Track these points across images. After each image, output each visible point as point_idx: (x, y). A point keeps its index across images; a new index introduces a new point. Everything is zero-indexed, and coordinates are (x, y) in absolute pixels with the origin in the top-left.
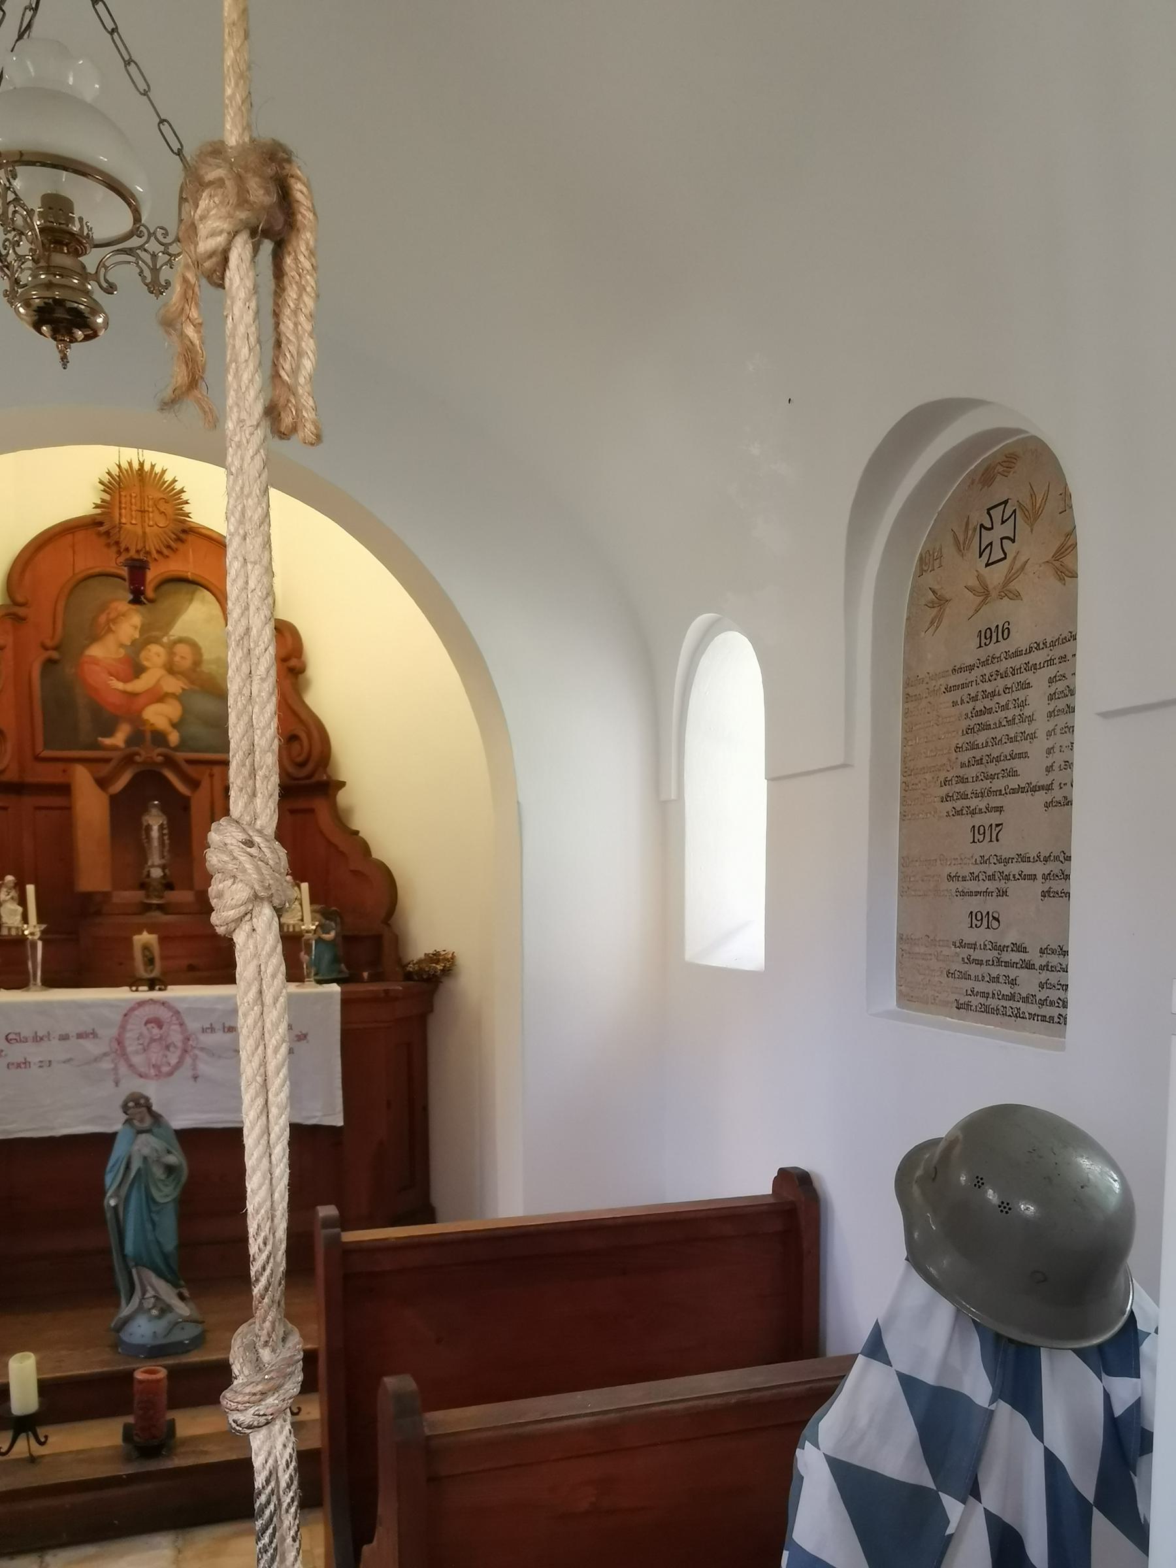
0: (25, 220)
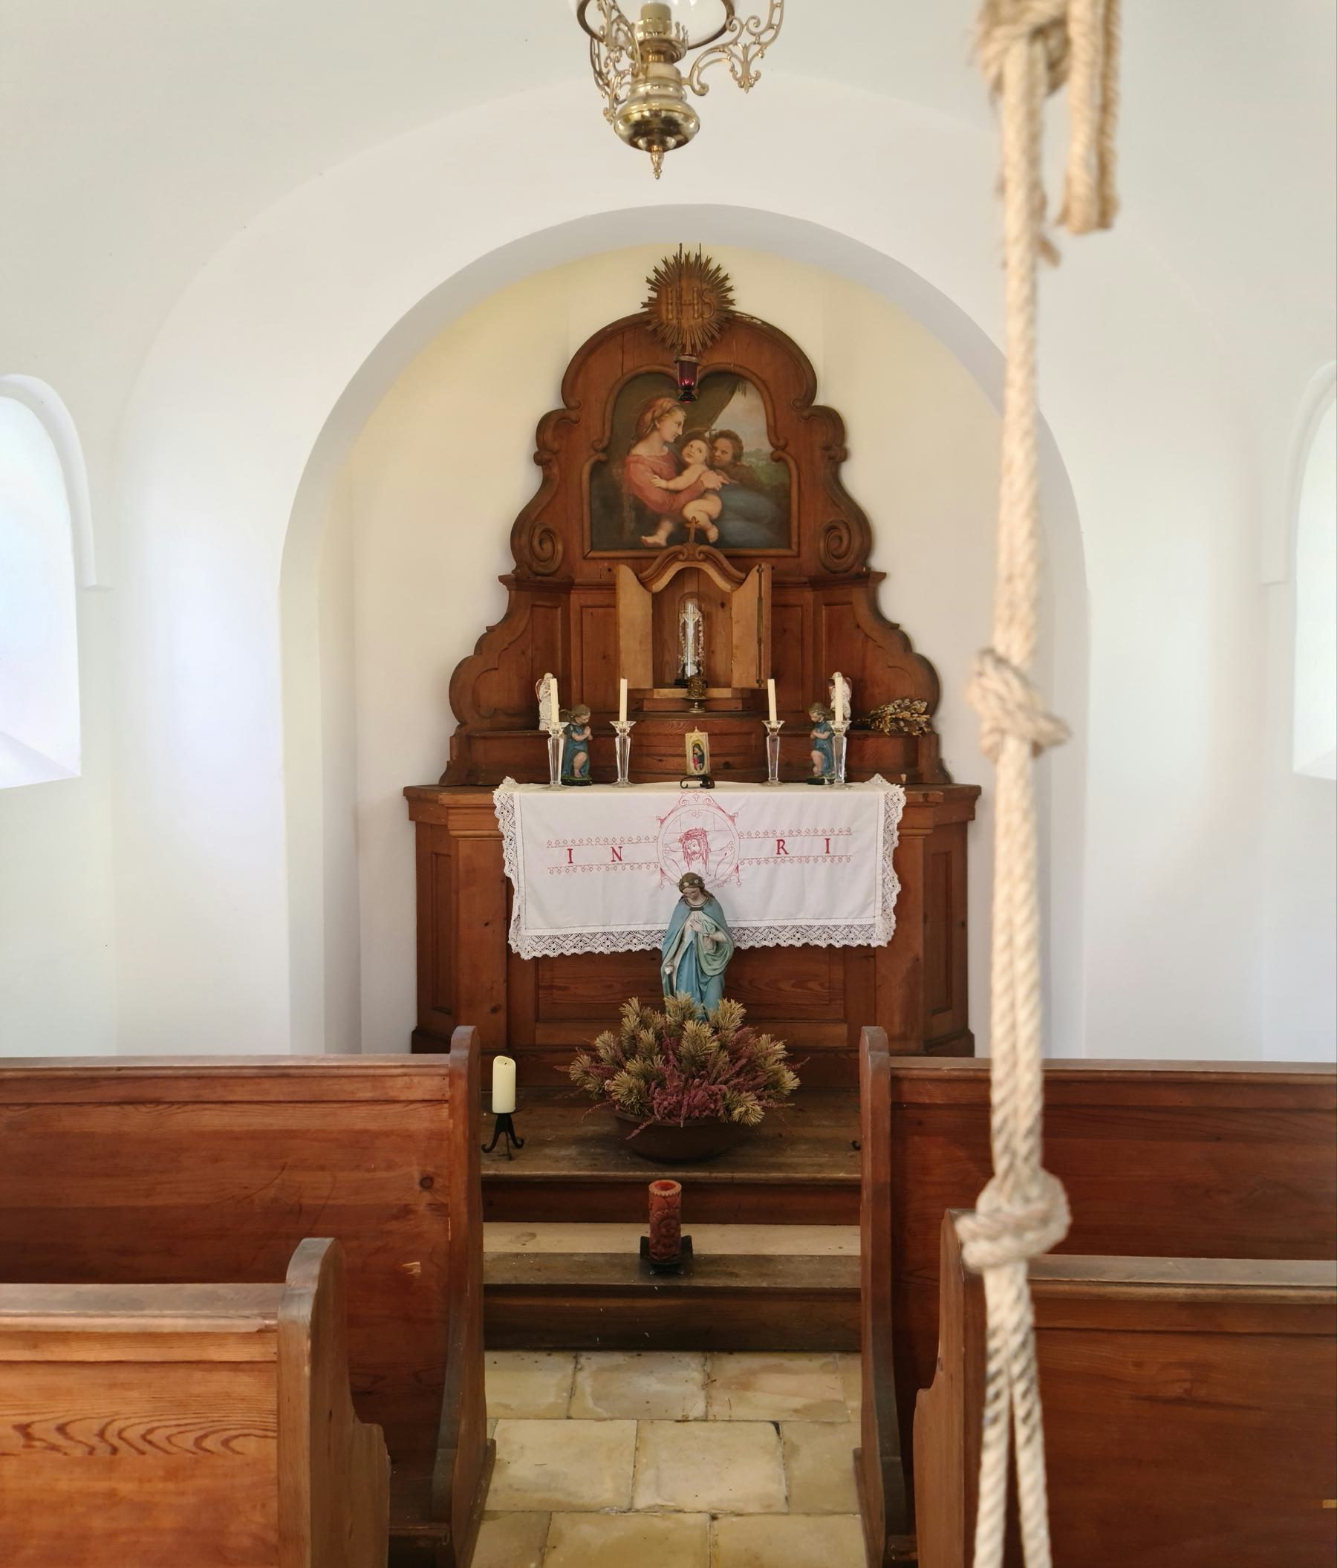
0: (626, 34)
